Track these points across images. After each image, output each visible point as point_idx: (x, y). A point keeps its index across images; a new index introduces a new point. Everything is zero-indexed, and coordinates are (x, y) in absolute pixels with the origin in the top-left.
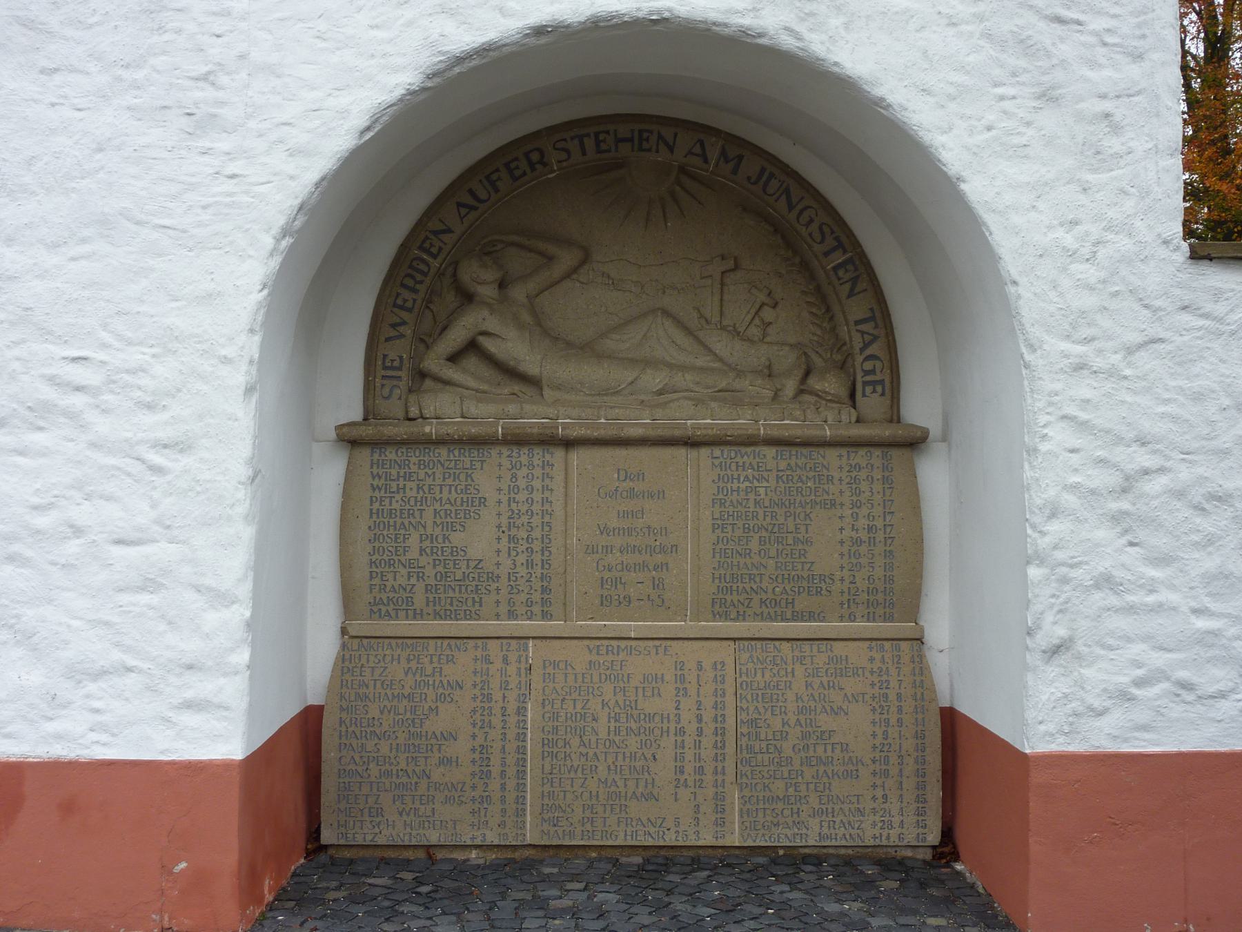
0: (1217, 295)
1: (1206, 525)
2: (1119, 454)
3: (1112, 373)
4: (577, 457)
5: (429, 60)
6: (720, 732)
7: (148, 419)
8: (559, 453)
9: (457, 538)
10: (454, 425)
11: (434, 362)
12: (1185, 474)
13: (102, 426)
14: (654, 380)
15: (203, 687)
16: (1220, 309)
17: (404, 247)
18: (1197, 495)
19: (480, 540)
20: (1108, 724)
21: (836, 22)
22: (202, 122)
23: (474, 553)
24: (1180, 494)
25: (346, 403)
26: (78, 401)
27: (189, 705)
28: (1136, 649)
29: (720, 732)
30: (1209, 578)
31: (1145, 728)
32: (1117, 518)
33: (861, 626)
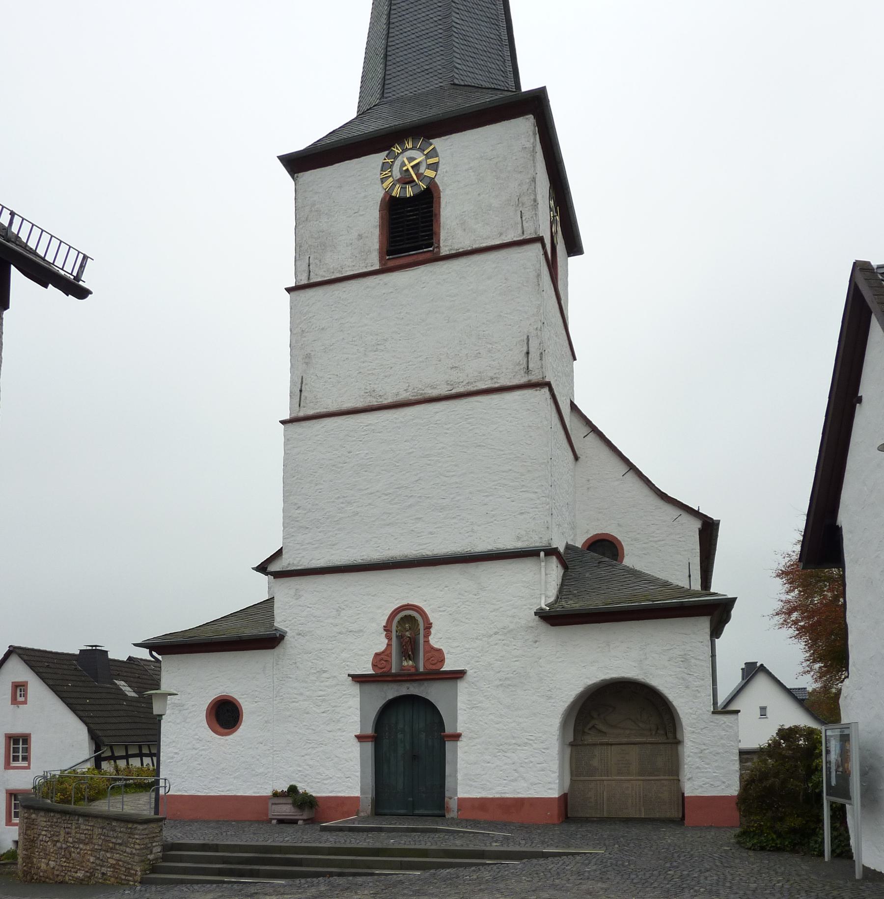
1: (716, 758)
3: (699, 733)
4: (613, 747)
11: (586, 730)
12: (712, 750)
13: (535, 746)
14: (628, 732)
15: (552, 786)
19: (595, 762)
22: (550, 698)
25: (571, 738)
32: (700, 757)
33: (666, 777)
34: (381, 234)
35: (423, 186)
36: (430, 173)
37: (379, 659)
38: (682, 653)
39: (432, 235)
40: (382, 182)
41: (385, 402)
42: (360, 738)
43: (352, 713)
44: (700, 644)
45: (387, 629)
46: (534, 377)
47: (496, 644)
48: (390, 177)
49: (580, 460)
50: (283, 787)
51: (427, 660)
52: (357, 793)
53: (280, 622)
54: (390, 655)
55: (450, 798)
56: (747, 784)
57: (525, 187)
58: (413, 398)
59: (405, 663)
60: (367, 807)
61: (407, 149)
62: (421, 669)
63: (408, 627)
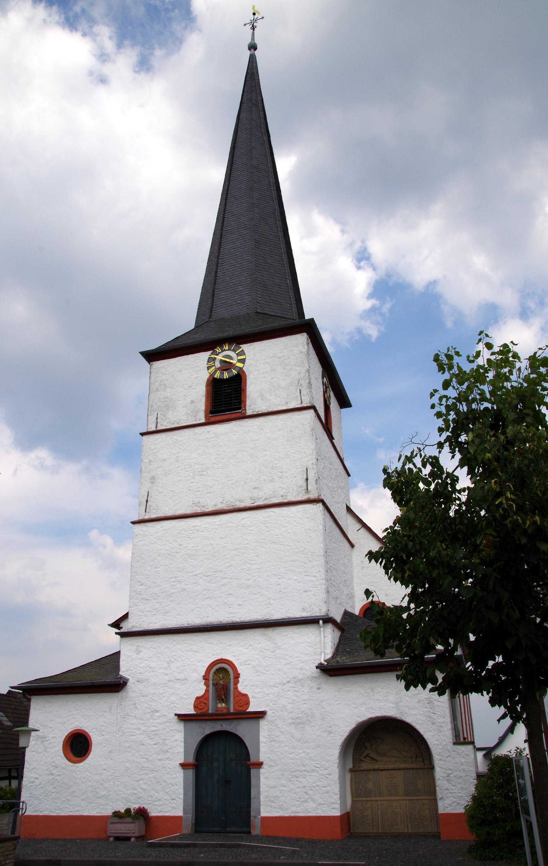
0: (457, 749)
1: (459, 781)
2: (447, 771)
3: (445, 760)
4: (383, 772)
5: (356, 723)
7: (326, 771)
8: (380, 772)
11: (362, 758)
12: (456, 774)
13: (320, 772)
15: (335, 806)
16: (458, 751)
18: (458, 777)
19: (370, 785)
20: (449, 808)
21: (406, 715)
22: (330, 733)
24: (455, 777)
25: (350, 765)
26: (317, 769)
30: (460, 788)
31: (453, 809)
32: (447, 780)
37: (199, 702)
52: (179, 812)
54: (207, 699)
55: (255, 817)
59: (219, 705)
60: (187, 827)
62: (232, 710)
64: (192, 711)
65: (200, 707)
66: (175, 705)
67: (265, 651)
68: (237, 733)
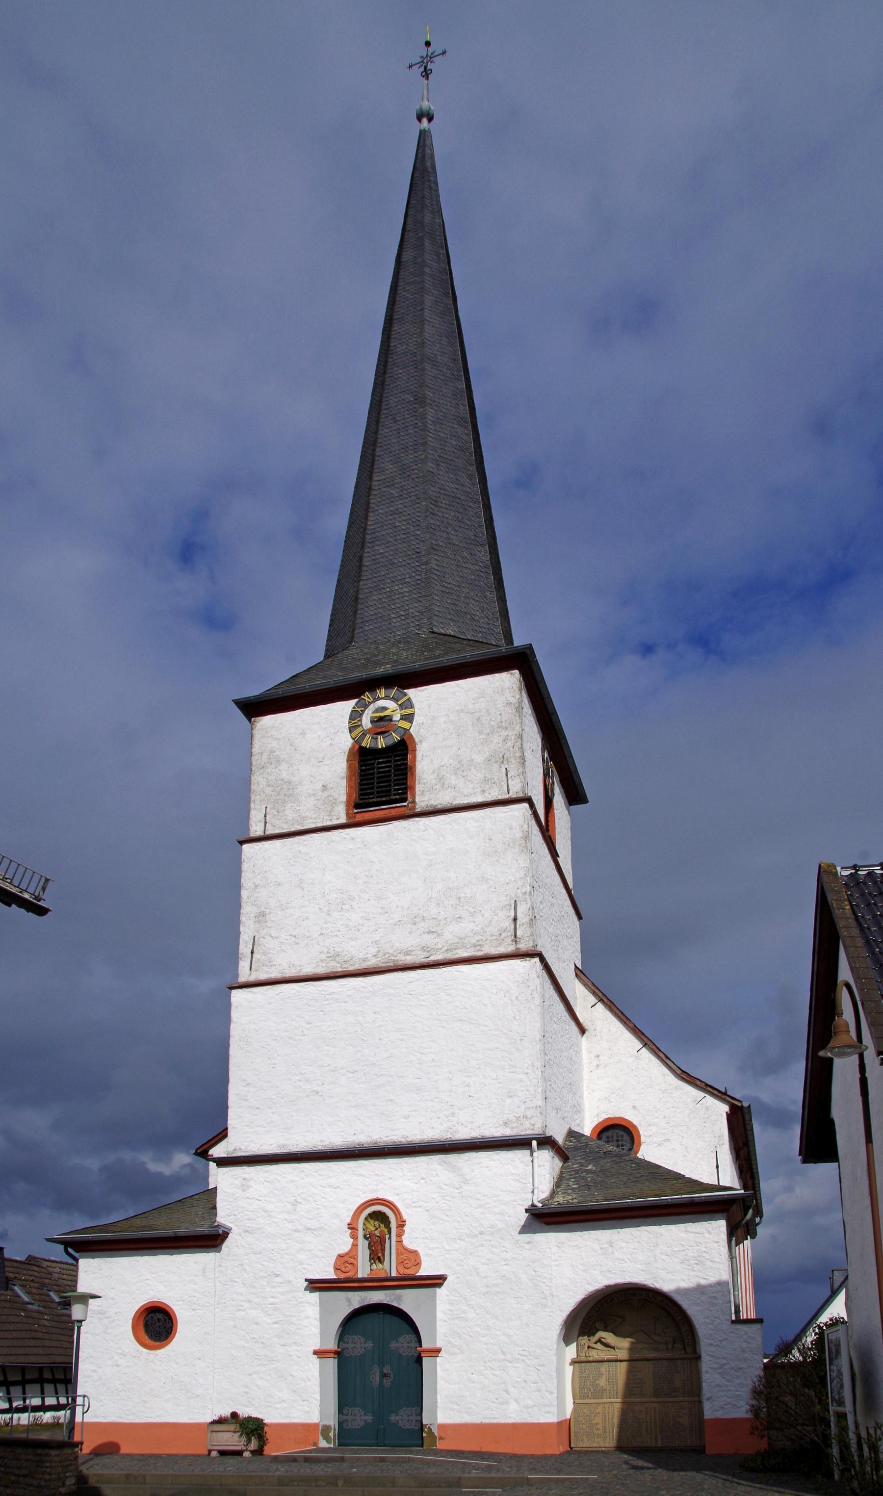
6: (655, 1422)
9: (597, 1382)
10: (596, 1357)
12: (733, 1365)
17: (590, 1311)
23: (602, 1385)
24: (731, 1368)
27: (548, 1412)
28: (724, 1398)
29: (655, 1422)
32: (720, 1373)
34: (349, 786)
35: (396, 737)
36: (404, 724)
37: (345, 1260)
38: (696, 1255)
39: (406, 789)
40: (351, 732)
41: (351, 968)
42: (319, 1353)
43: (313, 1322)
44: (715, 1244)
45: (352, 1227)
46: (524, 946)
47: (482, 1245)
48: (359, 726)
49: (587, 1033)
50: (226, 1412)
51: (400, 1263)
53: (223, 1217)
54: (355, 1257)
56: (755, 1411)
57: (510, 744)
58: (384, 965)
61: (379, 699)
62: (394, 1274)
63: (378, 1222)
64: (332, 1275)
65: (343, 1269)
66: (305, 1266)
67: (446, 1187)
68: (402, 1307)
